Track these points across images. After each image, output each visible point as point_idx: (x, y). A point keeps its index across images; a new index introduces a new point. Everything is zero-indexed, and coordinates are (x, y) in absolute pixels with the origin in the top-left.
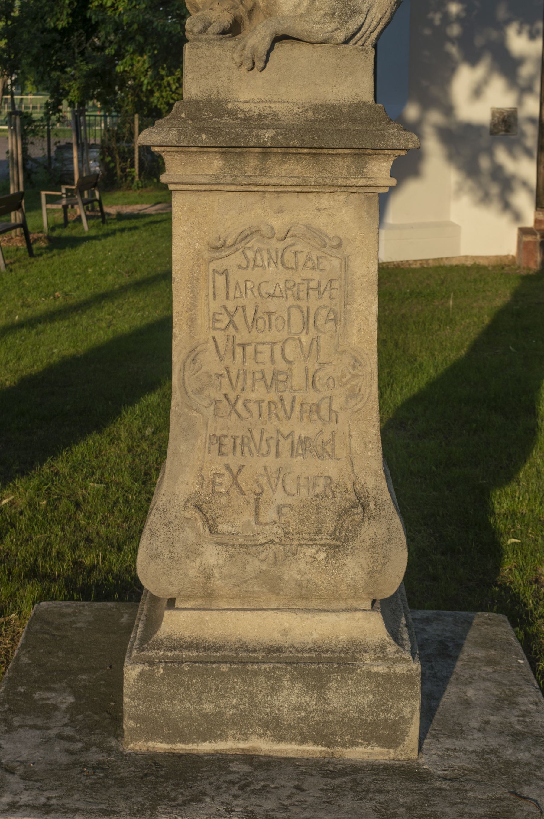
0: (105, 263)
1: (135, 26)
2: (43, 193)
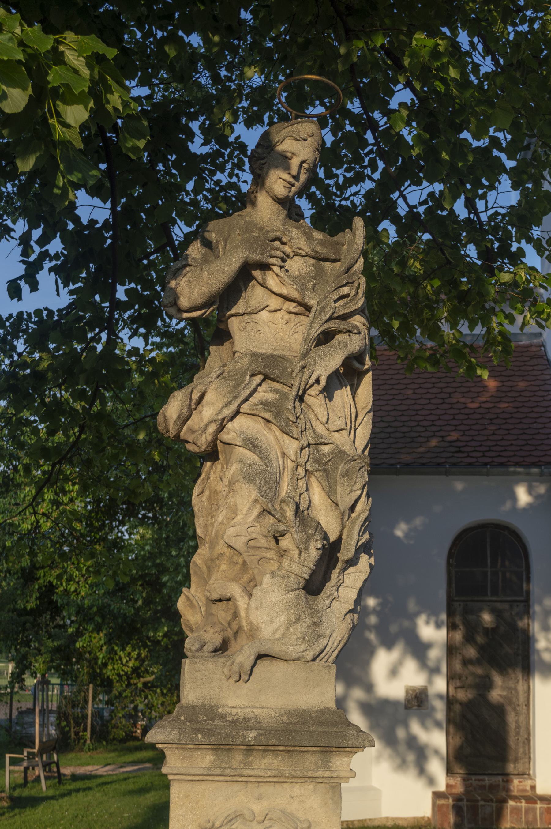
0: (62, 822)
1: (95, 609)
2: (8, 756)
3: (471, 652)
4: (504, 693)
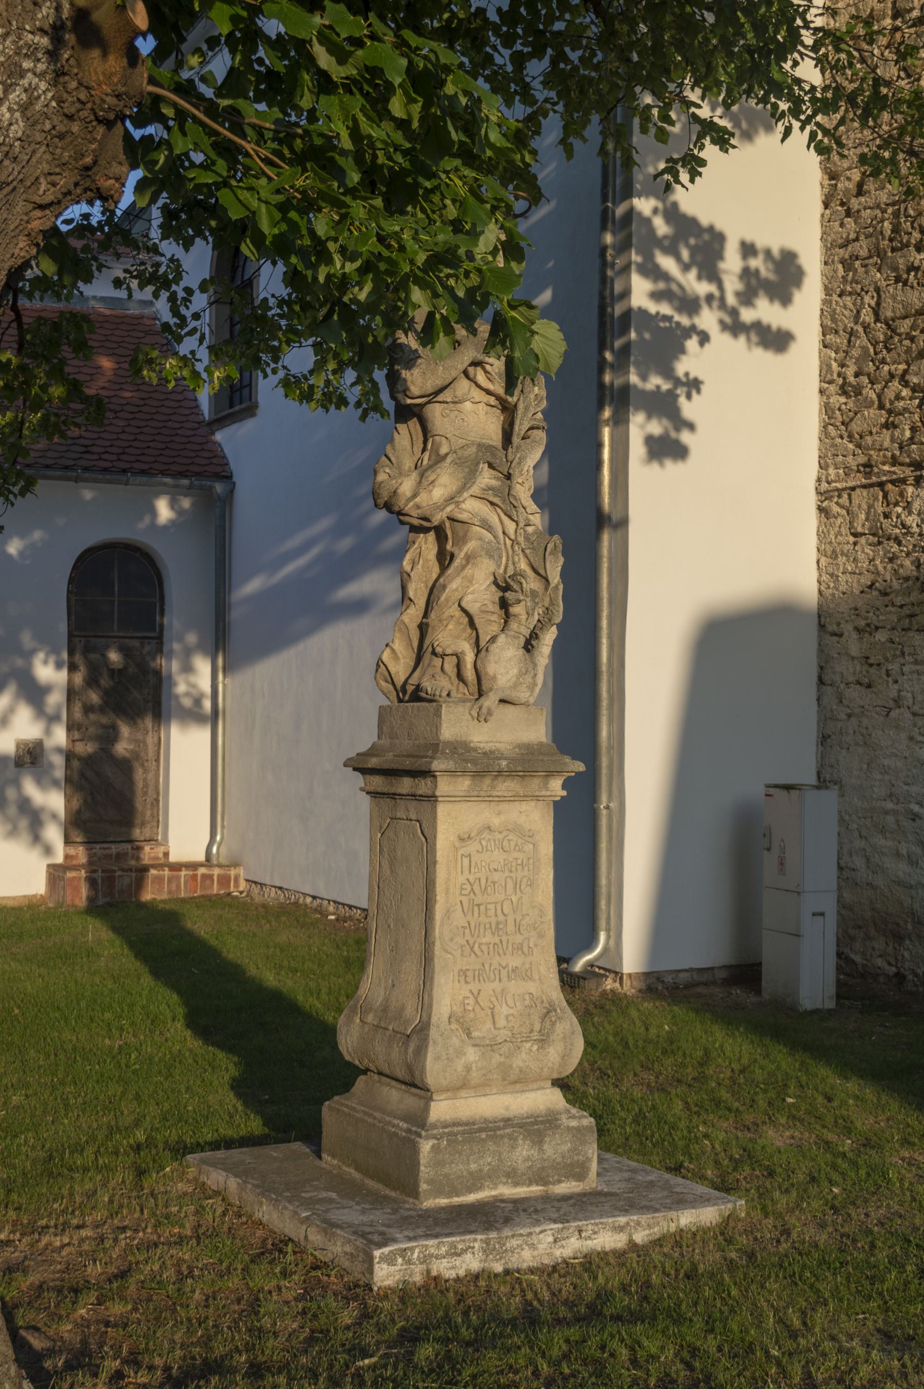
3: (94, 697)
4: (132, 747)
